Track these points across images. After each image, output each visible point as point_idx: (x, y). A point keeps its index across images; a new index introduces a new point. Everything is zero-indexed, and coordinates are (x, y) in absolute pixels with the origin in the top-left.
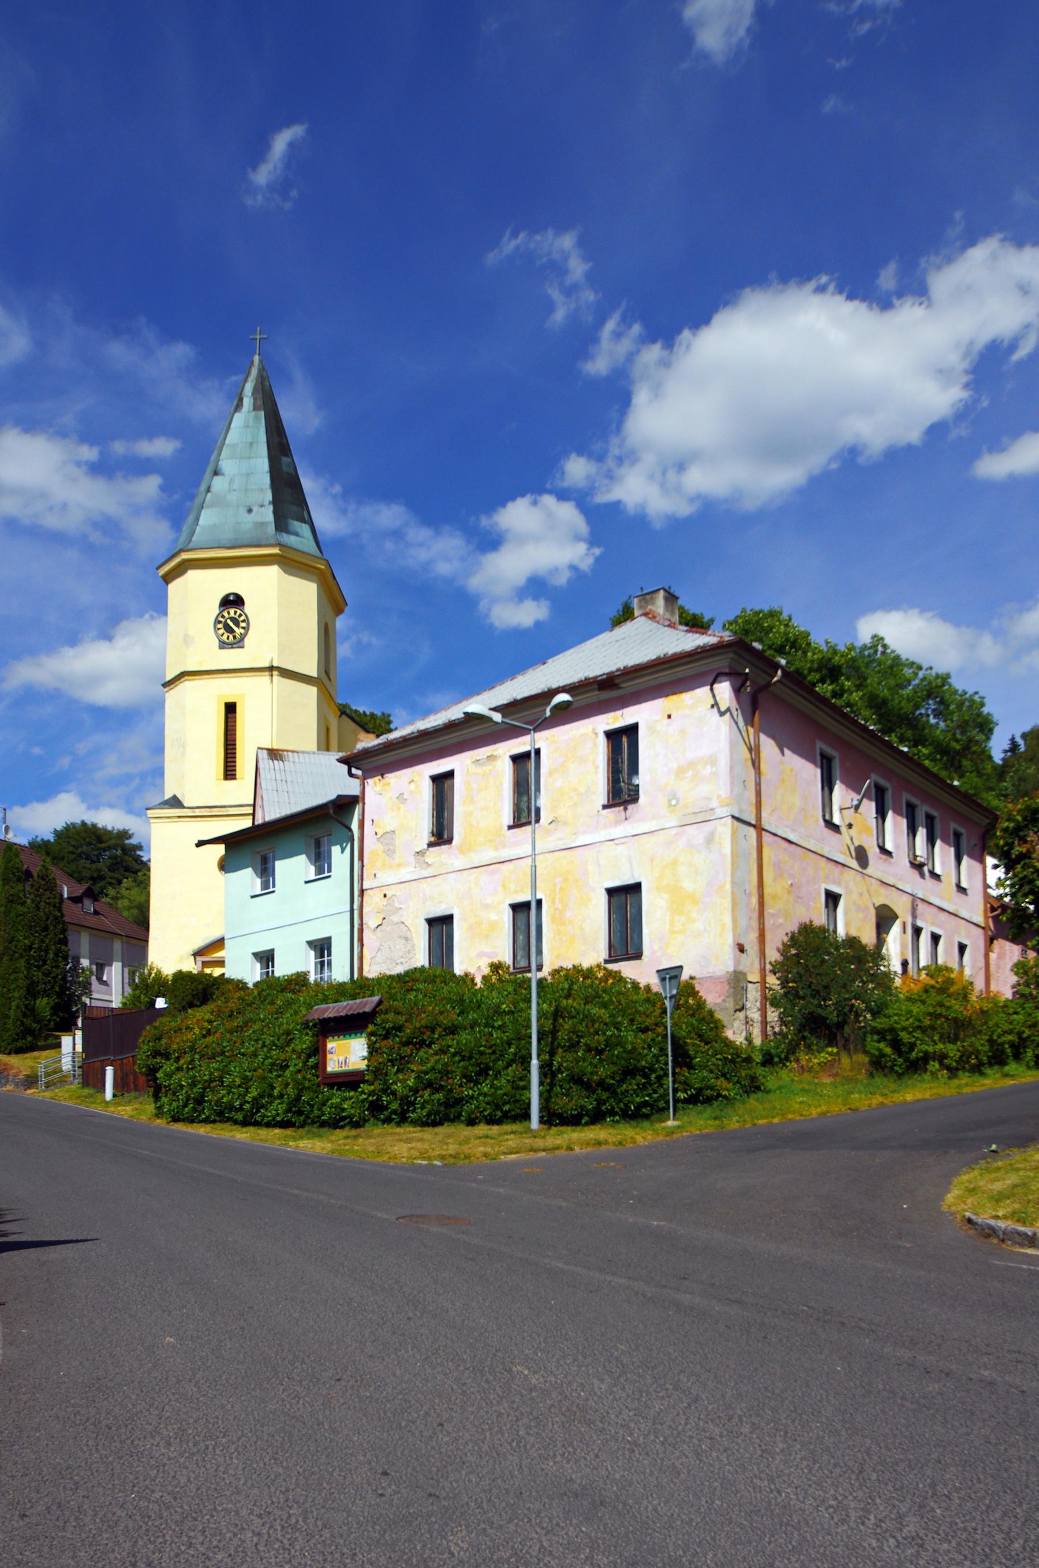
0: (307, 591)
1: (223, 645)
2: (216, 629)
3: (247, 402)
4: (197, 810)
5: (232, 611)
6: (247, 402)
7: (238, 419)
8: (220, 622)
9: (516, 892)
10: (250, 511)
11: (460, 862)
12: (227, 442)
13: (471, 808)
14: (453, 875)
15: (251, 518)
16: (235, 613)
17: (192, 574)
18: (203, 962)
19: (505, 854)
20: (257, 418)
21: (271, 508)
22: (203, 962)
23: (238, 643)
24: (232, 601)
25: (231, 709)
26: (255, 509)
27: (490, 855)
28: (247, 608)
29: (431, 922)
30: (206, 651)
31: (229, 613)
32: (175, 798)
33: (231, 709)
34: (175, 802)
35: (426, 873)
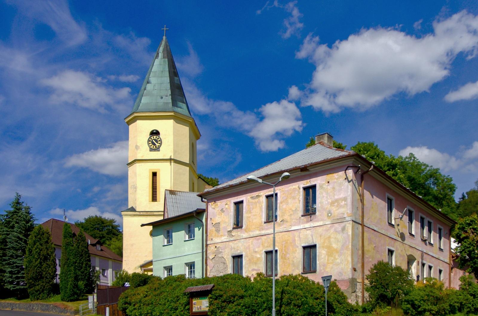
0: (185, 130)
1: (151, 150)
2: (148, 144)
3: (161, 55)
4: (141, 213)
5: (155, 137)
6: (161, 55)
7: (157, 62)
8: (150, 141)
9: (267, 247)
10: (162, 98)
11: (245, 235)
12: (152, 70)
13: (250, 215)
14: (243, 240)
15: (162, 101)
16: (156, 137)
17: (138, 122)
18: (144, 270)
19: (263, 232)
20: (164, 61)
21: (170, 97)
22: (144, 270)
23: (157, 149)
24: (155, 133)
25: (154, 174)
26: (164, 97)
27: (257, 233)
28: (161, 136)
29: (234, 257)
30: (144, 152)
31: (153, 137)
32: (132, 207)
33: (154, 174)
34: (133, 209)
35: (232, 239)
